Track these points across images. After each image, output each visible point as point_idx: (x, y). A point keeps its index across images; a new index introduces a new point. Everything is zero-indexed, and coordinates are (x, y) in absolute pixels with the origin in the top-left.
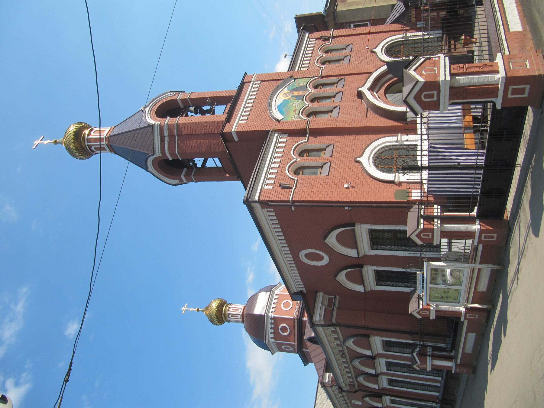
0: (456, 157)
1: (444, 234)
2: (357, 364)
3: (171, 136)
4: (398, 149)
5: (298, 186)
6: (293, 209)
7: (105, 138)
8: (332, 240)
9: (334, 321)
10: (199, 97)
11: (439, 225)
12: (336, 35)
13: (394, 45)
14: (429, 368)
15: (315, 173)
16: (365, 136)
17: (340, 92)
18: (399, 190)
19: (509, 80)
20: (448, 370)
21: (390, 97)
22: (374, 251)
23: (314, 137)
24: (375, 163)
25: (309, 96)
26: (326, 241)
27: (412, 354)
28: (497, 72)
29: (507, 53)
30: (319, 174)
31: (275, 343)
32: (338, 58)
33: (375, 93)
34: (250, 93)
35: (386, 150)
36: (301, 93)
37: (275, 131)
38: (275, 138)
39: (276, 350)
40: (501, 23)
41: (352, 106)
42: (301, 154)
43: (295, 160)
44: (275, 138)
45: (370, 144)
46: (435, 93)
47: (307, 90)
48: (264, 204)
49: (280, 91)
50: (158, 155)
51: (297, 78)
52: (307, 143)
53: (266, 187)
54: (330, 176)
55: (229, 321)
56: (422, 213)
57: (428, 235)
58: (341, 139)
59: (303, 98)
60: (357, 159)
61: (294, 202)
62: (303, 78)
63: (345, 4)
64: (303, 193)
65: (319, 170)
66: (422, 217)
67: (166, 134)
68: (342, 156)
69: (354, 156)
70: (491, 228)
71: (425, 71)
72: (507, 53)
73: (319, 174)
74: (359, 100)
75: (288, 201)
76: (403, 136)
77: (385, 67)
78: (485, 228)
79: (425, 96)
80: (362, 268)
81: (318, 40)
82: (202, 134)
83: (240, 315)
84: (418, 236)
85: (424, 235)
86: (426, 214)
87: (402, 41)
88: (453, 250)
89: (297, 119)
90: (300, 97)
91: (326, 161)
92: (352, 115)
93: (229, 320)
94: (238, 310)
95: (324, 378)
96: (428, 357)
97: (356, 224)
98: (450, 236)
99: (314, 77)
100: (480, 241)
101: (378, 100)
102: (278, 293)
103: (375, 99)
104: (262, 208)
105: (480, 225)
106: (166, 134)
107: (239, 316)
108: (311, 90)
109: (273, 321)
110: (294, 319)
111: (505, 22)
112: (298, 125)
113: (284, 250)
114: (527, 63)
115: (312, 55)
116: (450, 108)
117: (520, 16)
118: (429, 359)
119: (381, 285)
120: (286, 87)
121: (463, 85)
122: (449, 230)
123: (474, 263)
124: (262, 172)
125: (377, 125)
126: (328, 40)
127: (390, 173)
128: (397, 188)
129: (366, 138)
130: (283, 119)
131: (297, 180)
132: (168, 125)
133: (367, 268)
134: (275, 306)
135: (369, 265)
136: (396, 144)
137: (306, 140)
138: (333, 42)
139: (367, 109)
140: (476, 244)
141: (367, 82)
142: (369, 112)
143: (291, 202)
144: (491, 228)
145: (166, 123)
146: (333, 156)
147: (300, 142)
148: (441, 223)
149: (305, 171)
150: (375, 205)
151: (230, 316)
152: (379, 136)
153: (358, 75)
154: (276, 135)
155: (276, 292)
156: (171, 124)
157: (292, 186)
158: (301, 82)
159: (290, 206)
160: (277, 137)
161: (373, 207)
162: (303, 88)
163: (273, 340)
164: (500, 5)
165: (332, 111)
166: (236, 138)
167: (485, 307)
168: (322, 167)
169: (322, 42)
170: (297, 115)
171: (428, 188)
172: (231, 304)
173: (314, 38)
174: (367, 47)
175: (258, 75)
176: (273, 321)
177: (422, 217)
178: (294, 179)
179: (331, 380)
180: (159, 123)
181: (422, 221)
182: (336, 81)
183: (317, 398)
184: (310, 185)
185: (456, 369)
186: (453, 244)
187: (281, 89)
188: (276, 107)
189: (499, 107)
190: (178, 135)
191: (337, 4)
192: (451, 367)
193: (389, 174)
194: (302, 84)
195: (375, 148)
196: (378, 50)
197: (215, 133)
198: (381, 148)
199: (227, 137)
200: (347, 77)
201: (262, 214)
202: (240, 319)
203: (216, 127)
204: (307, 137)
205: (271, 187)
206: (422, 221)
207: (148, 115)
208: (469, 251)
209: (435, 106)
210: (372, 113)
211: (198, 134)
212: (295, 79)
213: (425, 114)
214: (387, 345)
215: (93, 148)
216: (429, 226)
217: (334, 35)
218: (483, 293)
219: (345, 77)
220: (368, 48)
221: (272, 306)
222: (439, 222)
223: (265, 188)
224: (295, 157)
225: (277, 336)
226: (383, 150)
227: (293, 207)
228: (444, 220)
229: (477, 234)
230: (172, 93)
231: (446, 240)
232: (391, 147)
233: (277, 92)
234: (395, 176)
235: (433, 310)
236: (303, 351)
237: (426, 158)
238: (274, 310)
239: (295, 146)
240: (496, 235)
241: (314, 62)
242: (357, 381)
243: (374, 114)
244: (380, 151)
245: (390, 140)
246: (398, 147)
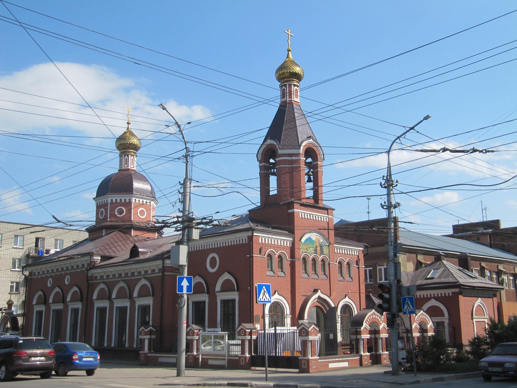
0: (280, 346)
1: (243, 341)
2: (121, 285)
3: (292, 162)
4: (282, 315)
5: (261, 258)
6: (247, 256)
7: (291, 100)
8: (226, 276)
9: (166, 273)
10: (319, 178)
11: (248, 338)
12: (360, 269)
13: (350, 309)
14: (141, 337)
15: (268, 267)
16: (290, 295)
17: (318, 277)
18: (260, 317)
19: (308, 360)
20: (142, 348)
21: (314, 309)
22: (220, 301)
23: (290, 264)
24: (276, 303)
25: (317, 257)
26: (226, 272)
27: (152, 326)
28: (312, 357)
29: (319, 361)
30: (268, 269)
32: (343, 273)
33: (317, 300)
34: (320, 216)
35: (281, 308)
36: (319, 251)
37: (294, 239)
39: (98, 202)
40: (333, 360)
41: (309, 286)
42: (280, 257)
43: (276, 254)
44: (290, 239)
45: (285, 299)
46: (305, 335)
47: (320, 256)
48: (251, 238)
49: (321, 237)
50: (279, 152)
51: (329, 248)
52: (286, 260)
53: (260, 238)
54: (267, 276)
55: (121, 156)
56: (253, 331)
57: (191, 334)
58: (289, 284)
59: (315, 254)
60: (277, 292)
61: (252, 257)
62: (329, 251)
63: (405, 260)
64: (257, 262)
65: (270, 269)
66: (251, 331)
67: (293, 158)
68: (278, 283)
69: (279, 290)
70: (247, 361)
71: (313, 331)
72: (319, 361)
73: (268, 269)
74: (313, 290)
75: (253, 254)
76: (290, 318)
77: (333, 305)
78: (247, 358)
79: (304, 331)
80: (207, 294)
81: (357, 257)
82: (293, 185)
83: (128, 167)
84: (242, 329)
85: (191, 332)
86: (253, 332)
87: (353, 315)
88: (231, 347)
89: (301, 251)
90: (316, 251)
91: (275, 273)
92: (303, 286)
95: (97, 255)
96: (150, 336)
97: (239, 292)
98: (243, 345)
99: (329, 259)
100: (240, 357)
101: (312, 302)
102: (151, 204)
103: (312, 301)
104: (248, 237)
105: (248, 357)
106: (293, 158)
107: (127, 166)
108: (321, 258)
109: (127, 201)
110: (131, 221)
111: (333, 361)
112: (297, 253)
113: (217, 243)
114: (315, 367)
115: (346, 255)
116: (300, 340)
117: (336, 367)
118: (148, 337)
119: (193, 304)
120: (323, 240)
121: (307, 345)
122: (245, 343)
123: (228, 356)
124: (269, 235)
125: (296, 302)
126: (357, 264)
127: (269, 312)
128: (261, 316)
129: (289, 296)
130: (302, 242)
131: (265, 257)
132: (299, 160)
133: (207, 297)
134: (141, 202)
135: (209, 298)
136: (285, 314)
137: (288, 259)
138: (355, 268)
139: (307, 296)
140: (238, 356)
141: (324, 295)
142: (305, 297)
143: (252, 255)
144: (247, 361)
145: (301, 158)
146: (278, 277)
147: (287, 256)
148: (249, 340)
149: (269, 261)
150: (252, 304)
151: (126, 157)
152: (290, 304)
153: (329, 288)
154: (291, 239)
155: (152, 202)
156: (300, 162)
157: (261, 254)
158: (326, 250)
159: (250, 254)
160: (290, 240)
161: (250, 303)
162: (322, 252)
163: (110, 201)
164: (342, 361)
165: (306, 273)
166: (290, 211)
167: (200, 364)
168: (272, 271)
169: (356, 260)
170: (304, 251)
171: (260, 333)
173: (359, 254)
174: (349, 292)
175: (333, 219)
176: (127, 201)
177: (251, 331)
178: (265, 255)
179: (95, 261)
180: (301, 153)
181: (249, 330)
182: (326, 274)
183: (15, 225)
184: (262, 265)
185: (142, 353)
186: (235, 346)
187: (322, 238)
189: (299, 358)
190: (292, 167)
191: (405, 254)
192: (144, 350)
193: (268, 311)
194: (325, 251)
195: (283, 302)
196: (347, 299)
197: (294, 195)
198: (283, 306)
199: (291, 205)
200: (329, 281)
201: (244, 235)
202: (124, 167)
203: (297, 195)
204: (290, 259)
205: (260, 242)
206: (249, 330)
208: (230, 353)
209: (300, 335)
210: (304, 299)
211: (293, 181)
212: (329, 246)
213: (298, 331)
214: (144, 309)
215: (284, 87)
216: (247, 334)
217: (360, 268)
218: (208, 363)
219: (329, 279)
220: (349, 292)
221: (140, 200)
222: (249, 338)
223: (260, 238)
224: (278, 253)
225: (114, 205)
226: (282, 307)
227: (249, 256)
228: (250, 341)
229: (244, 356)
230: (322, 157)
231: (240, 343)
232: (283, 311)
233: (320, 235)
234: (267, 315)
235: (194, 337)
236: (103, 229)
237: (280, 332)
238: (137, 202)
239: (285, 252)
240: (244, 364)
241: (341, 256)
242: (100, 283)
243: (303, 300)
244: (281, 305)
245: (287, 310)
246: (283, 315)
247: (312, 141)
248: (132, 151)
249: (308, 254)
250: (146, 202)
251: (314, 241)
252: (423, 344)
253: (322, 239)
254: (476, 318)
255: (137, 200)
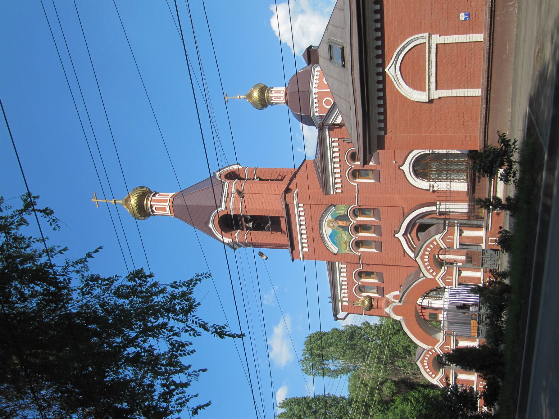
31: (320, 116)
38: (337, 266)
44: (337, 266)
49: (325, 219)
83: (283, 96)
93: (273, 103)
94: (281, 92)
151: (273, 98)
160: (338, 265)
172: (272, 88)
187: (326, 217)
188: (328, 237)
207: (227, 185)
233: (323, 221)
238: (318, 110)
247: (211, 224)
248: (266, 95)
249: (351, 242)
250: (316, 80)
251: (332, 230)
252: (480, 159)
253: (327, 217)
254: (429, 89)
255: (315, 110)
